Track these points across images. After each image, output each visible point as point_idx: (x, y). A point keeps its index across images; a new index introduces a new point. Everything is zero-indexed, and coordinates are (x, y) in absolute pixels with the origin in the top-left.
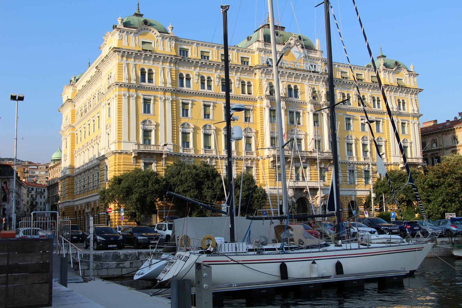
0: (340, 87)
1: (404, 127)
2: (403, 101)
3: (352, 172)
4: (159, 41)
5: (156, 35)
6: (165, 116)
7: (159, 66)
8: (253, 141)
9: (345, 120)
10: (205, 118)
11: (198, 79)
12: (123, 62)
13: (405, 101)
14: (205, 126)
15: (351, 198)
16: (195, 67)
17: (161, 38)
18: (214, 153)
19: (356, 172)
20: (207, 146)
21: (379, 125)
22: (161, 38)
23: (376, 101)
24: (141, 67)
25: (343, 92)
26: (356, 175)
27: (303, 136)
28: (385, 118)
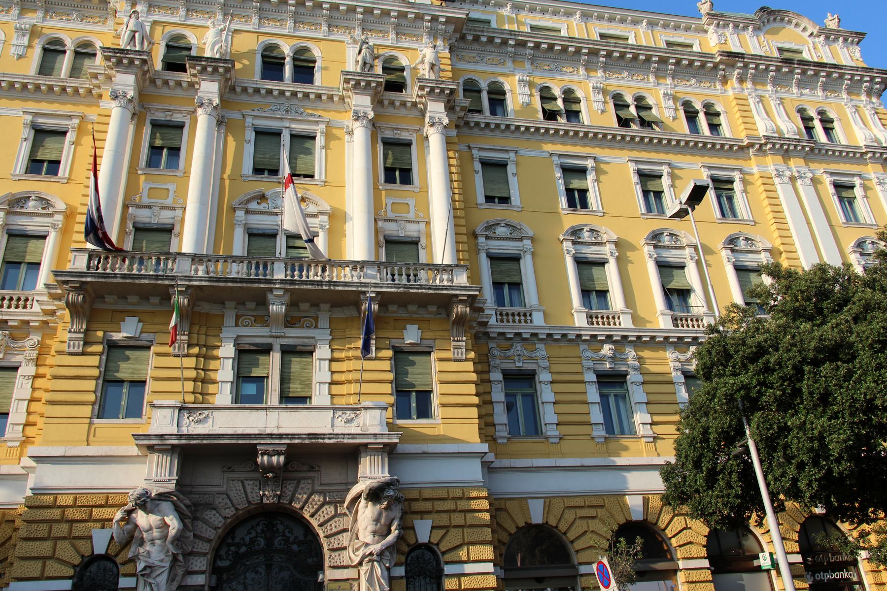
0: (528, 65)
1: (851, 201)
2: (821, 113)
3: (612, 381)
4: (819, 46)
5: (808, 33)
6: (809, 224)
7: (8, 19)
8: (611, 275)
9: (558, 174)
10: (649, 209)
11: (676, 110)
12: (746, 92)
13: (832, 115)
14: (655, 237)
15: (525, 510)
16: (589, 67)
17: (822, 38)
18: (626, 322)
19: (633, 377)
20: (595, 294)
21: (730, 199)
22: (822, 38)
23: (702, 117)
24: (796, 104)
25: (540, 81)
26: (637, 394)
27: (688, 251)
28: (755, 170)
